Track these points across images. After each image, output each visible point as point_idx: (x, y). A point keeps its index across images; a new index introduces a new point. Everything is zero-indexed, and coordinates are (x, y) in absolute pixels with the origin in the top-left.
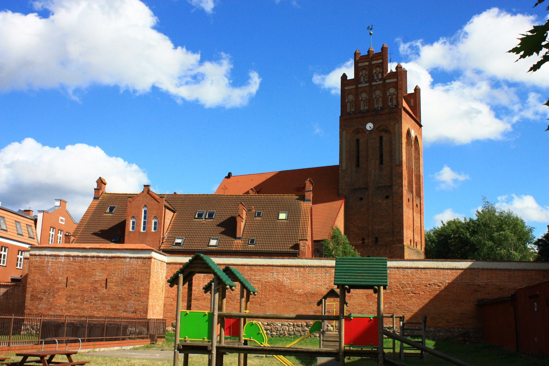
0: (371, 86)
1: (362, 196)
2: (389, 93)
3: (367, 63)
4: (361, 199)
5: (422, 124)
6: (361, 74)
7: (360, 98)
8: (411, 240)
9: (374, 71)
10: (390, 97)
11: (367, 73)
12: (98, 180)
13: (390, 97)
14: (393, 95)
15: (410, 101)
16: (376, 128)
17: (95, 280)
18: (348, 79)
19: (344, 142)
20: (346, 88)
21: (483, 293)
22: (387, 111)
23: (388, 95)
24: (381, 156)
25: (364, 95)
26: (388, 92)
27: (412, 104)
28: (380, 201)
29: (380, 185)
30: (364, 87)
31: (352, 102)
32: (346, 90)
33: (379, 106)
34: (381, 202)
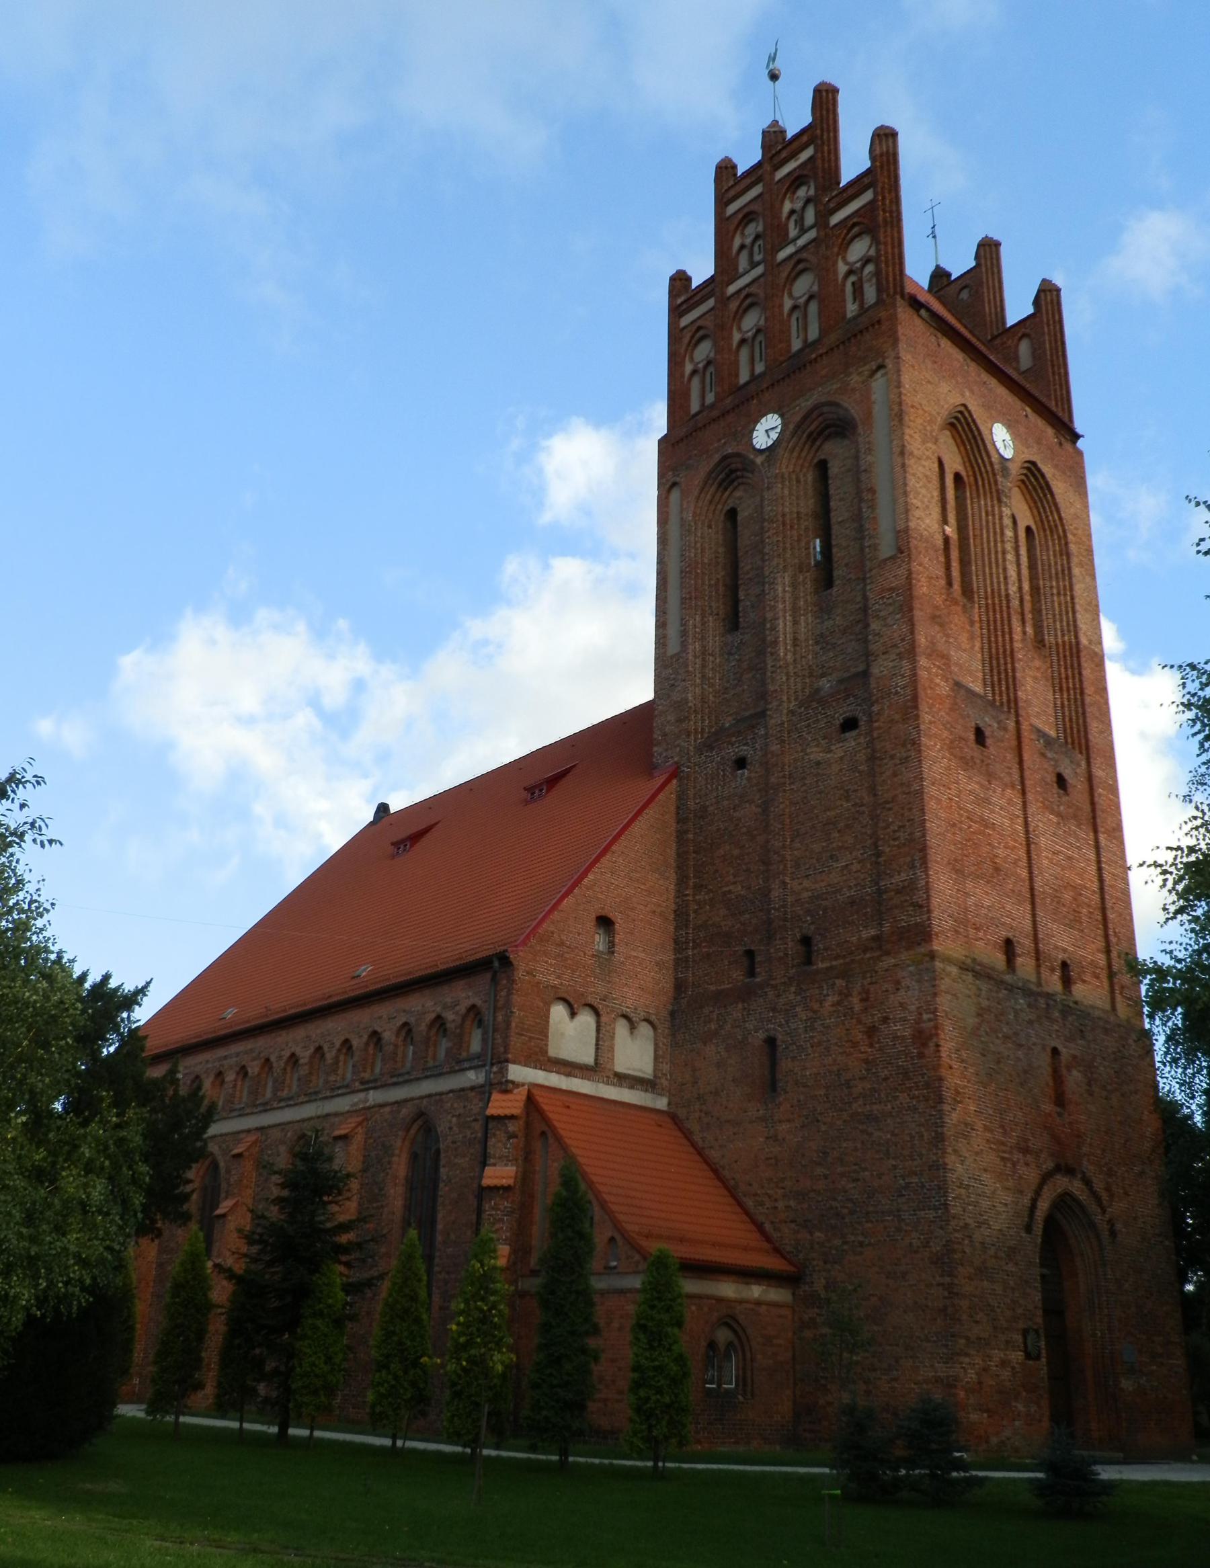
1: (744, 750)
5: (1079, 426)
16: (791, 427)
18: (694, 285)
28: (816, 754)
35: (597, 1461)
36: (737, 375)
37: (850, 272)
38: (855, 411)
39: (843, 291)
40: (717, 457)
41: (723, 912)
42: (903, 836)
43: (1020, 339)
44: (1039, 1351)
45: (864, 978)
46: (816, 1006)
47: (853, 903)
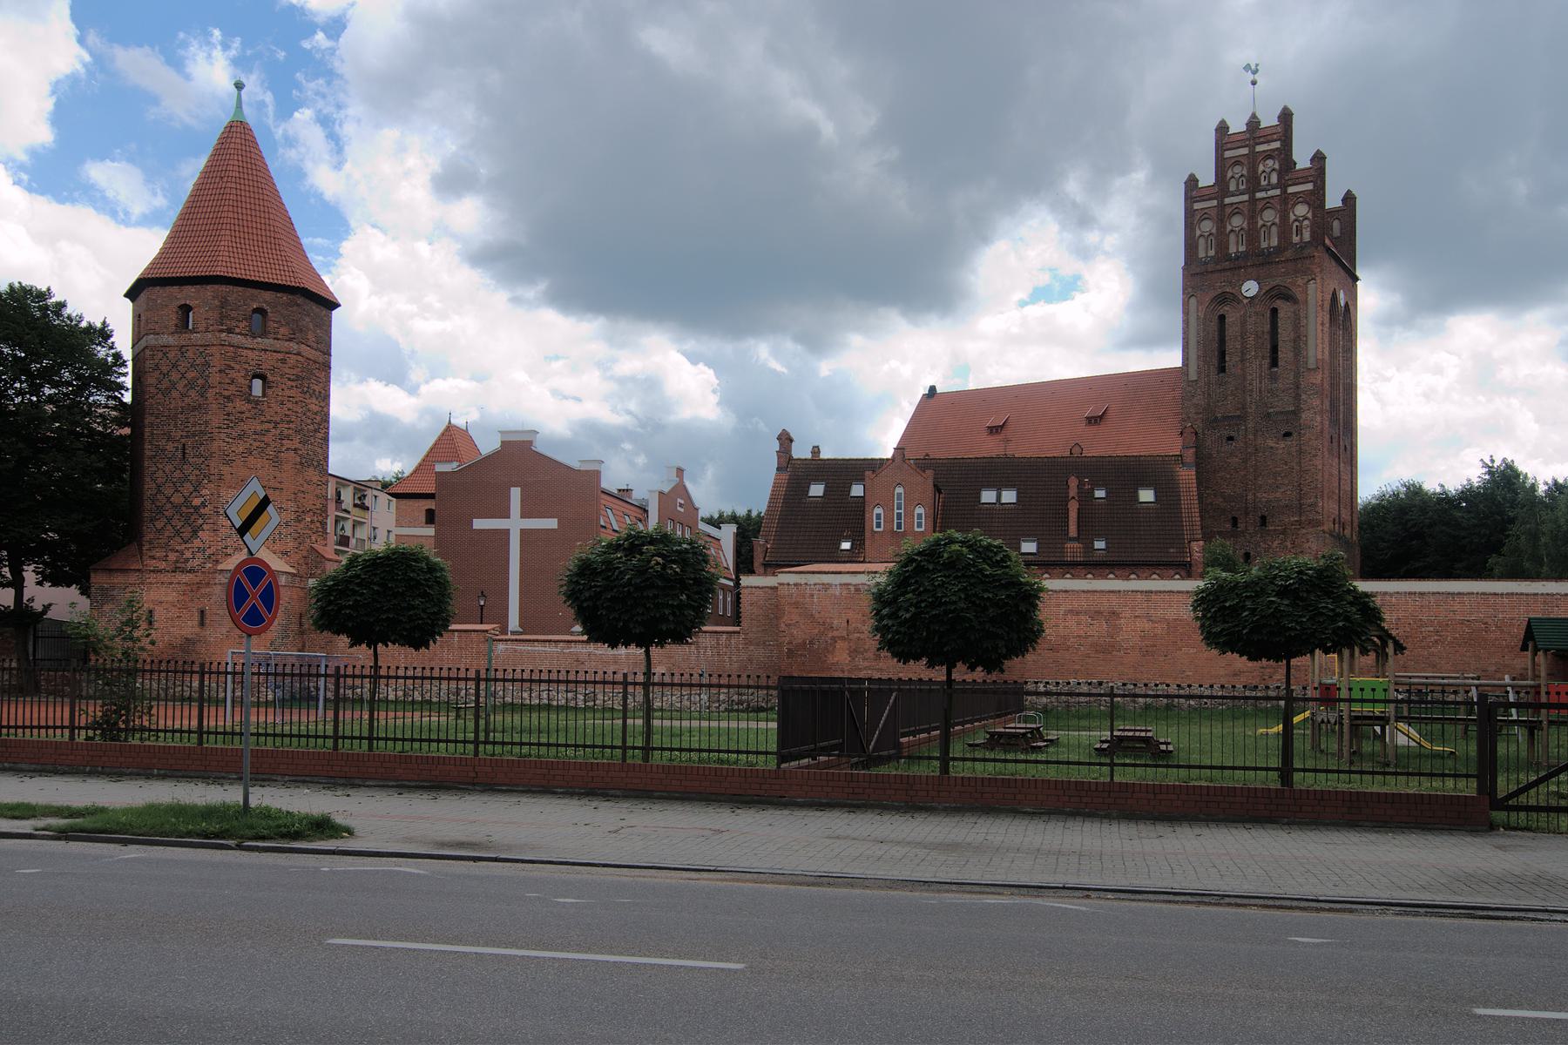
1: (1233, 434)
3: (1245, 151)
4: (1231, 438)
6: (1230, 174)
9: (1261, 168)
10: (1297, 223)
11: (1245, 172)
15: (1332, 226)
22: (1289, 254)
23: (1291, 221)
24: (1274, 349)
26: (1291, 214)
28: (1271, 443)
29: (1272, 410)
32: (1197, 210)
34: (1273, 445)
36: (1228, 249)
37: (1296, 220)
38: (1299, 296)
40: (1220, 291)
41: (1221, 500)
42: (1313, 485)
44: (325, 506)
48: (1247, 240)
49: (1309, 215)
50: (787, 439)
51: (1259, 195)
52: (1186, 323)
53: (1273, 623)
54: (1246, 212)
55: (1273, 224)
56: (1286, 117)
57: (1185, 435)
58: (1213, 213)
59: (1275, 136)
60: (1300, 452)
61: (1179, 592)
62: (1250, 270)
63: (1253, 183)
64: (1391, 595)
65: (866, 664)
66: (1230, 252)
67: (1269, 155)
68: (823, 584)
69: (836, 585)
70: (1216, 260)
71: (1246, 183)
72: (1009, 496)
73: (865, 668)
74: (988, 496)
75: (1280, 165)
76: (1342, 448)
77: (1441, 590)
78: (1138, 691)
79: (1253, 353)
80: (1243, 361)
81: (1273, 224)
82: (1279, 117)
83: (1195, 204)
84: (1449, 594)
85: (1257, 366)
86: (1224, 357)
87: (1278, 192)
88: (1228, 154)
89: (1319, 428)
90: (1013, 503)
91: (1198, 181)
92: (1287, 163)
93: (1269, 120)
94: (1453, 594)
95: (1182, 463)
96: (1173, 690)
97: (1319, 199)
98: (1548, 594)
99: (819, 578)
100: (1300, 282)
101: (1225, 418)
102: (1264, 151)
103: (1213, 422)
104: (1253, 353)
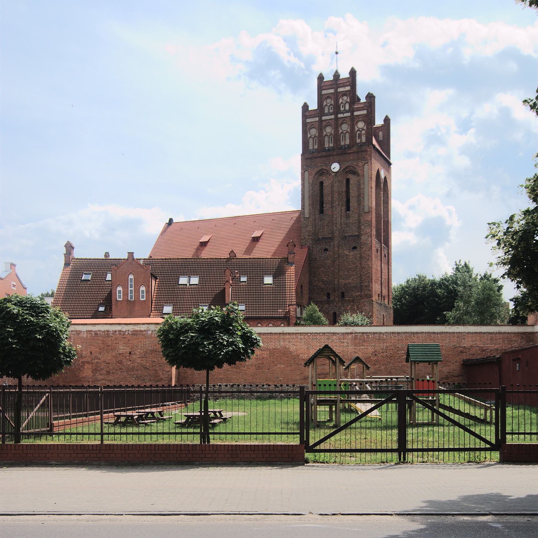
0: (337, 119)
1: (327, 247)
2: (358, 127)
3: (332, 91)
4: (326, 250)
5: (392, 161)
6: (325, 104)
7: (325, 133)
8: (379, 294)
9: (341, 101)
10: (358, 132)
11: (332, 103)
12: (66, 244)
13: (358, 132)
14: (362, 130)
15: (379, 134)
16: (342, 169)
17: (118, 353)
19: (307, 185)
20: (308, 120)
21: (468, 354)
22: (355, 149)
23: (356, 130)
24: (348, 201)
25: (329, 130)
26: (356, 127)
27: (381, 138)
28: (346, 252)
29: (347, 234)
30: (329, 120)
31: (314, 137)
32: (308, 123)
33: (346, 144)
34: (348, 253)
35: (500, 432)
38: (360, 172)
39: (356, 135)
40: (320, 168)
41: (321, 283)
42: (367, 275)
43: (380, 131)
45: (357, 303)
46: (346, 307)
47: (354, 287)
48: (333, 141)
49: (365, 128)
50: (70, 247)
51: (340, 116)
52: (303, 185)
53: (194, 348)
54: (333, 125)
55: (347, 132)
56: (353, 73)
57: (289, 247)
58: (317, 125)
59: (348, 84)
60: (361, 257)
61: (275, 334)
62: (335, 157)
63: (337, 110)
64: (383, 334)
65: (102, 377)
66: (326, 147)
67: (344, 94)
68: (76, 331)
69: (84, 332)
70: (318, 151)
71: (333, 109)
72: (195, 280)
73: (101, 380)
74: (183, 280)
75: (350, 99)
76: (383, 255)
77: (408, 331)
78: (254, 389)
79: (337, 203)
80: (332, 207)
81: (347, 132)
82: (350, 73)
83: (307, 119)
84: (412, 333)
85: (339, 210)
86: (323, 205)
87: (349, 114)
88: (324, 92)
89: (370, 245)
90: (197, 285)
91: (308, 107)
92: (355, 99)
93: (344, 74)
94: (414, 333)
95: (288, 262)
96: (272, 388)
97: (369, 119)
98: (459, 333)
99: (74, 328)
100: (360, 164)
101: (324, 238)
102: (342, 91)
103: (317, 240)
104: (337, 203)
